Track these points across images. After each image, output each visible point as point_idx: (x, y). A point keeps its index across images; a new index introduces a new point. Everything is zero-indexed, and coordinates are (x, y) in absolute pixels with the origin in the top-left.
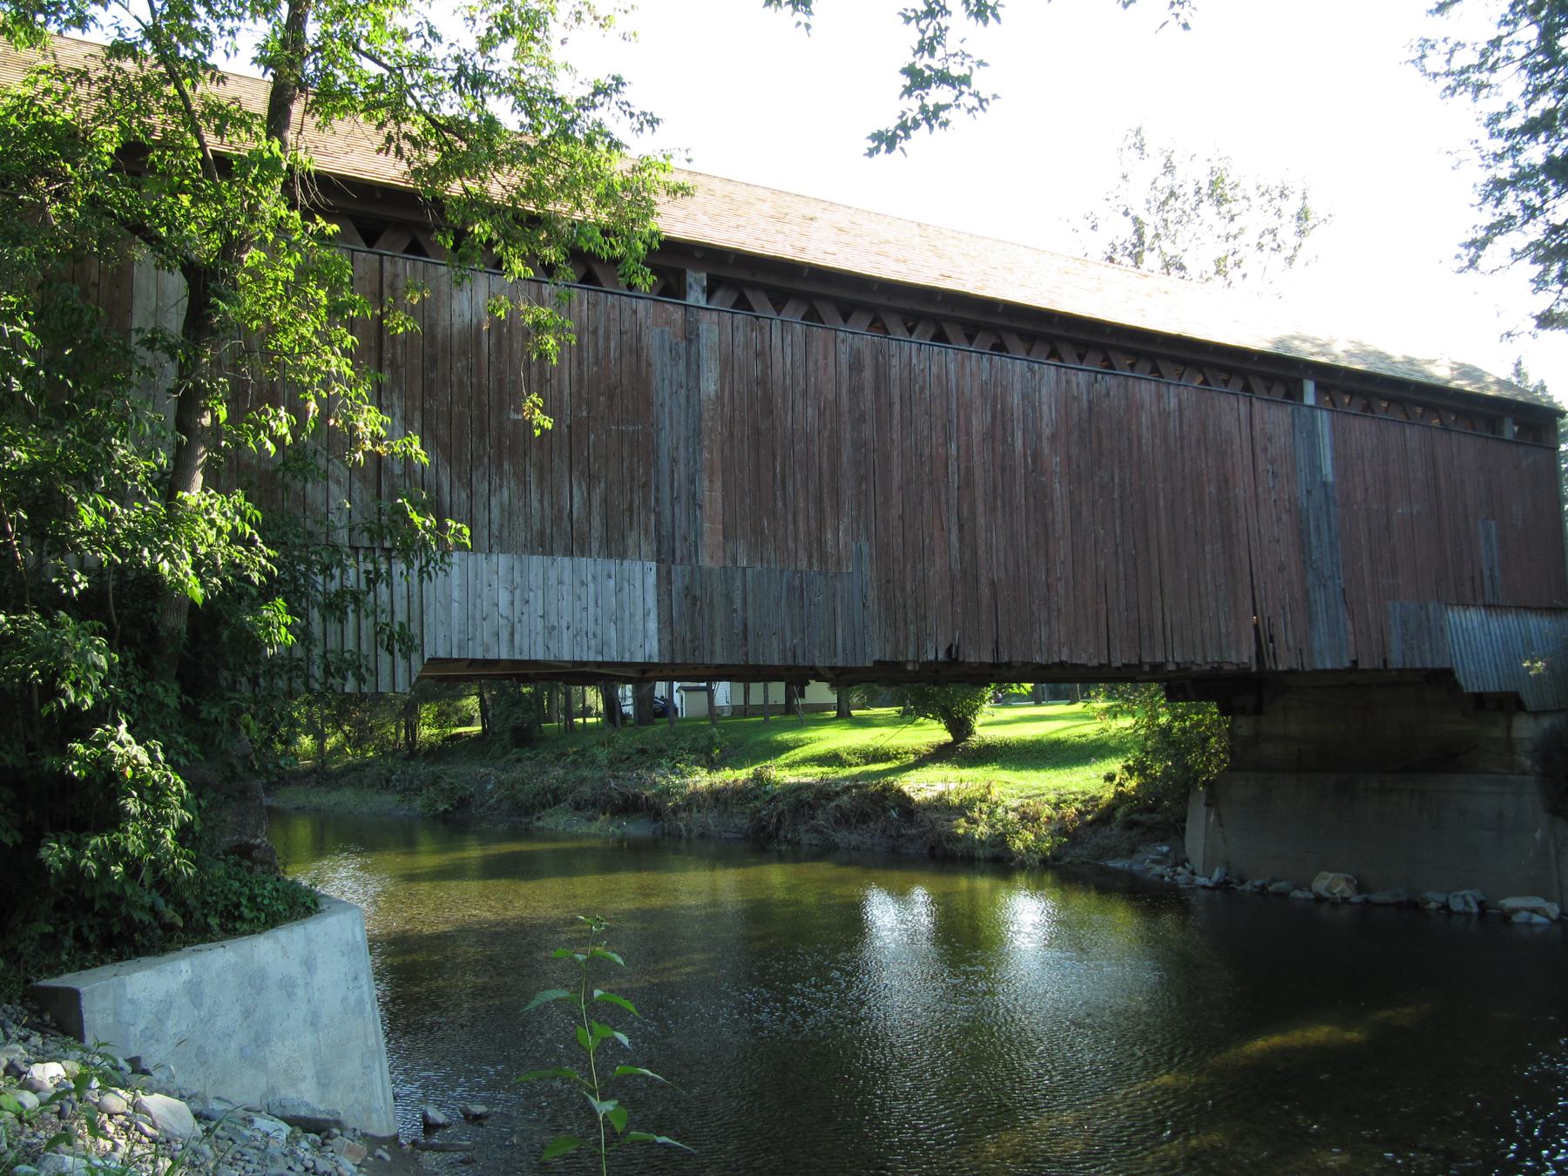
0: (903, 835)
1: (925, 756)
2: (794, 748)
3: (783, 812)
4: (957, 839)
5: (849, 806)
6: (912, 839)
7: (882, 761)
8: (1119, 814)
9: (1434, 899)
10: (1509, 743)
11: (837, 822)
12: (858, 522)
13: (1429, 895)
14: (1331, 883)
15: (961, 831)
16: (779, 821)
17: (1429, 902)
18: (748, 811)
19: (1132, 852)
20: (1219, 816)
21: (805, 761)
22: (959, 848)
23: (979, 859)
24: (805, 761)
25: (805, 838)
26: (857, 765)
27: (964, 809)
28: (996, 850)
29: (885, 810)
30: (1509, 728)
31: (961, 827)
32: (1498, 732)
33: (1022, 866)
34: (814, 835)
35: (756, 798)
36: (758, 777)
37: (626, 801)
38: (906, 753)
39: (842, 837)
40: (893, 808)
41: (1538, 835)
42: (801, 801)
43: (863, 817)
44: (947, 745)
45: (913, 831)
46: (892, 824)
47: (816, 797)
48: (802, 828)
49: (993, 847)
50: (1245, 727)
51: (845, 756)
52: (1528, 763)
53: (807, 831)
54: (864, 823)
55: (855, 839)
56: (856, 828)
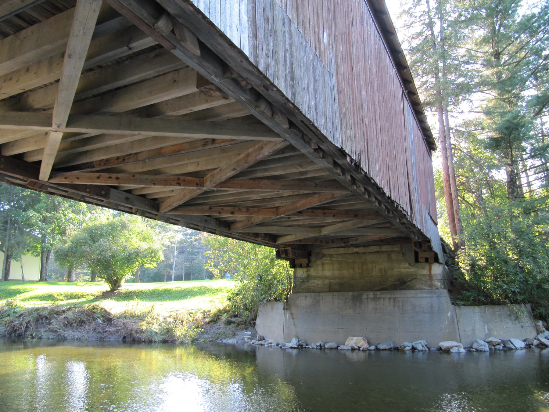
0: (106, 332)
1: (97, 296)
2: (23, 292)
3: (29, 322)
4: (142, 332)
5: (72, 317)
6: (112, 334)
7: (75, 298)
8: (224, 317)
9: (408, 346)
10: (430, 276)
11: (65, 326)
12: (368, 30)
13: (406, 344)
14: (354, 341)
15: (144, 328)
16: (27, 327)
17: (405, 347)
18: (4, 323)
19: (234, 335)
20: (292, 314)
21: (32, 298)
22: (143, 337)
23: (155, 342)
24: (32, 298)
25: (45, 335)
26: (62, 300)
27: (141, 318)
28: (164, 337)
29: (94, 319)
30: (430, 270)
31: (144, 326)
32: (425, 272)
33: (182, 343)
34: (51, 333)
35: (9, 315)
36: (9, 304)
37: (507, 128)
38: (88, 295)
39: (69, 333)
40: (99, 318)
41: (449, 314)
42: (40, 316)
43: (82, 323)
44: (107, 292)
45: (112, 329)
46: (99, 326)
47: (49, 313)
48: (42, 330)
49: (162, 335)
50: (302, 272)
51: (56, 296)
52: (439, 284)
53: (46, 331)
54: (81, 326)
55: (77, 334)
56: (77, 328)
